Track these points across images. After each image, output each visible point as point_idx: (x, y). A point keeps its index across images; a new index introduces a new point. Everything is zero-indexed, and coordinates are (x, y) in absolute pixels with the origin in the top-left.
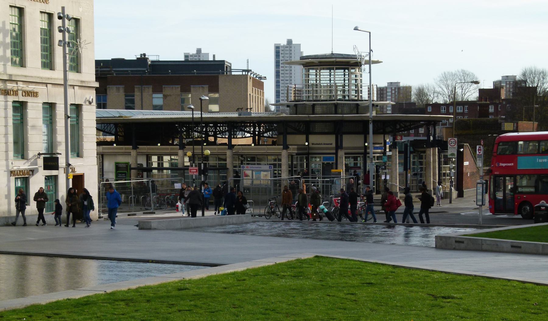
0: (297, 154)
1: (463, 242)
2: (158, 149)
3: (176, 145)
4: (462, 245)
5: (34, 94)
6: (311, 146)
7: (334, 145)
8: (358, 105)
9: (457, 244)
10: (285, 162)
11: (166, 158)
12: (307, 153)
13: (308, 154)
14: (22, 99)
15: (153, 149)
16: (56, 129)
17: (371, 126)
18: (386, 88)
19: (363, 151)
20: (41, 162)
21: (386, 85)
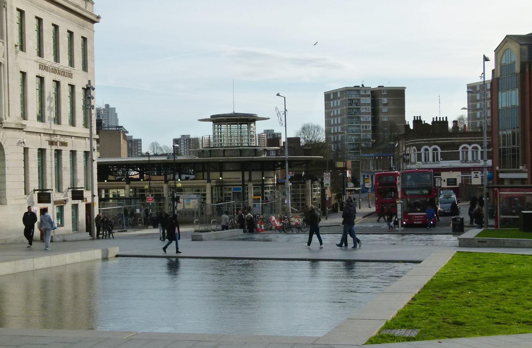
0: (216, 186)
1: (486, 242)
2: (106, 184)
3: (124, 181)
4: (485, 244)
5: (64, 144)
6: (224, 180)
7: (241, 179)
8: (256, 150)
9: (480, 243)
10: (208, 192)
11: (111, 191)
12: (221, 185)
13: (222, 186)
14: (59, 148)
15: (137, 184)
16: (76, 170)
17: (287, 164)
18: (180, 139)
19: (241, 184)
20: (70, 194)
21: (180, 137)
